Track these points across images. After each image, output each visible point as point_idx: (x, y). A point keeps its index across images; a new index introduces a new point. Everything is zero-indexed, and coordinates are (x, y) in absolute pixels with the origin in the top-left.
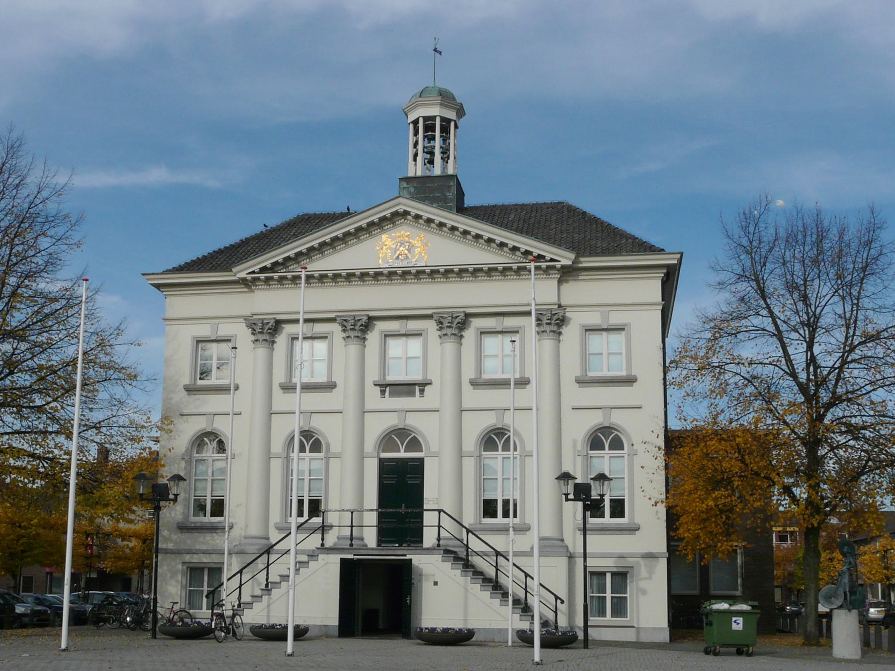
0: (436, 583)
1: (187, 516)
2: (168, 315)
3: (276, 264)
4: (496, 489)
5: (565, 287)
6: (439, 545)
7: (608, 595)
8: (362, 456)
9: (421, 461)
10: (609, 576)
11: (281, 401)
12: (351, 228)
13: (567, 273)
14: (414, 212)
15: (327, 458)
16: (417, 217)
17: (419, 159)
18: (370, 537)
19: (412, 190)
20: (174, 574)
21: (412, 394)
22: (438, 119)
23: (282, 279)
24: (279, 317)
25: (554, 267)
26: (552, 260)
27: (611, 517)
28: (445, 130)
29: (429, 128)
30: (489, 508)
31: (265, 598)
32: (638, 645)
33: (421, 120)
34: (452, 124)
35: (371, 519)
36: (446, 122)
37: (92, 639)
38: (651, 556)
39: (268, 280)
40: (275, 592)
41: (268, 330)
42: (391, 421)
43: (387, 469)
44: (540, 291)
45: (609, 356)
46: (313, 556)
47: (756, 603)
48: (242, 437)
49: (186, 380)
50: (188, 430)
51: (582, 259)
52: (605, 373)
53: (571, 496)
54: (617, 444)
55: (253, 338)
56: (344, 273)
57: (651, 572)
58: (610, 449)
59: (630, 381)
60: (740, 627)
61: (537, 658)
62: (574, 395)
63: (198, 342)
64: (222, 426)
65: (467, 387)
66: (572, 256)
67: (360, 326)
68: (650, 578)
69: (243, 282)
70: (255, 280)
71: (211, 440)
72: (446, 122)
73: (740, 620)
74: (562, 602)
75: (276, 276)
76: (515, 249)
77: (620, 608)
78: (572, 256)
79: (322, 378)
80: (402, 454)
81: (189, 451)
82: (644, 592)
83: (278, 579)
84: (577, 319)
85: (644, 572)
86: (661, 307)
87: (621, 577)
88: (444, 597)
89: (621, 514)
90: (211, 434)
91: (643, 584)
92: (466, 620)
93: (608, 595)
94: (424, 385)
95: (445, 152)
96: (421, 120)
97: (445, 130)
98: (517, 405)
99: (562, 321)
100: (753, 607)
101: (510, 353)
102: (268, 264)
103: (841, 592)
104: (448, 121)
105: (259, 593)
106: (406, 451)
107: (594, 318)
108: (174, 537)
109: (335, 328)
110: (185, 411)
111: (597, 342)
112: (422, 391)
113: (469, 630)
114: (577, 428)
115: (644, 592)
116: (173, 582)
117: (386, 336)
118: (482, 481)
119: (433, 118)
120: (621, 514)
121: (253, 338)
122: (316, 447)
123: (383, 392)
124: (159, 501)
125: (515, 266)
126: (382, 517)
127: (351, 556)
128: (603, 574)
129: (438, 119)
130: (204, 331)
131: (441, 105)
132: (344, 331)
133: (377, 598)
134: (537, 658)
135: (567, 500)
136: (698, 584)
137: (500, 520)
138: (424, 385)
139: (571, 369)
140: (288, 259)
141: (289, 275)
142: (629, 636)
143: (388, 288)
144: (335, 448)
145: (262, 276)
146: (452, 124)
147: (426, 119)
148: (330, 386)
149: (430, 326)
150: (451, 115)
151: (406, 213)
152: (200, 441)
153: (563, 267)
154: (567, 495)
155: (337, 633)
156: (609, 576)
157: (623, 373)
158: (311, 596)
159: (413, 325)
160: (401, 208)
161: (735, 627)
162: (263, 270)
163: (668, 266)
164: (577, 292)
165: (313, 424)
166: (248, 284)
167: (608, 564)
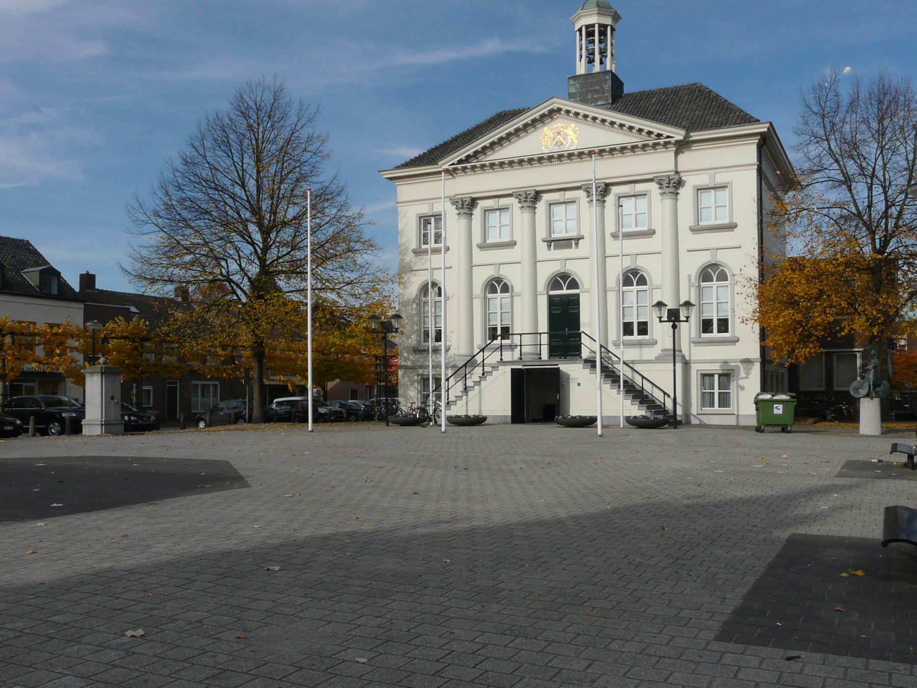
0: (579, 384)
1: (419, 342)
2: (399, 200)
3: (468, 157)
4: (632, 315)
5: (681, 157)
6: (521, 359)
7: (716, 391)
8: (535, 295)
9: (577, 296)
10: (716, 377)
11: (479, 256)
12: (528, 120)
13: (682, 146)
14: (565, 108)
15: (512, 297)
16: (568, 112)
17: (583, 59)
18: (545, 355)
19: (578, 85)
20: (412, 383)
21: (570, 247)
22: (597, 26)
23: (473, 168)
24: (608, 181)
25: (669, 143)
26: (668, 137)
27: (719, 332)
28: (603, 33)
29: (590, 34)
30: (628, 329)
31: (464, 397)
32: (738, 427)
33: (584, 28)
34: (609, 28)
35: (545, 339)
36: (602, 28)
37: (321, 426)
38: (747, 361)
39: (464, 169)
40: (471, 393)
41: (468, 205)
42: (556, 268)
43: (553, 302)
44: (661, 162)
45: (715, 209)
46: (495, 367)
47: (794, 394)
48: (453, 284)
49: (414, 246)
50: (415, 282)
51: (691, 134)
52: (713, 222)
53: (665, 318)
54: (723, 277)
55: (457, 212)
56: (607, 149)
57: (748, 374)
58: (717, 280)
59: (731, 227)
60: (780, 412)
61: (599, 433)
62: (688, 240)
63: (550, 204)
64: (439, 277)
65: (475, 250)
66: (683, 132)
67: (532, 198)
68: (747, 378)
69: (447, 171)
70: (455, 170)
71: (431, 288)
72: (602, 28)
73: (781, 407)
74: (669, 396)
75: (469, 165)
76: (640, 131)
77: (725, 401)
78: (683, 132)
79: (506, 239)
80: (565, 291)
81: (418, 296)
82: (742, 388)
83: (472, 384)
84: (691, 181)
85: (742, 374)
86: (756, 167)
87: (726, 376)
88: (586, 393)
89: (726, 331)
90: (635, 272)
91: (741, 382)
92: (480, 411)
93: (716, 391)
94: (578, 239)
95: (603, 53)
96: (584, 28)
97: (603, 33)
98: (624, 253)
99: (680, 183)
100: (792, 397)
101: (508, 223)
102: (463, 157)
103: (866, 385)
104: (605, 26)
105: (460, 394)
106: (567, 289)
107: (703, 180)
108: (411, 357)
109: (513, 201)
110: (415, 268)
111: (708, 198)
112: (577, 244)
113: (591, 417)
114: (691, 266)
115: (742, 388)
116: (412, 389)
117: (619, 198)
118: (486, 316)
119: (593, 26)
120: (726, 331)
121: (457, 212)
122: (505, 289)
123: (549, 246)
124: (386, 333)
125: (640, 144)
126: (551, 337)
127: (520, 367)
128: (712, 375)
129: (597, 26)
130: (424, 209)
131: (598, 14)
132: (660, 188)
133: (538, 396)
134: (310, 429)
135: (661, 321)
136: (824, 378)
137: (715, 334)
138: (578, 239)
139: (686, 219)
140: (476, 153)
141: (478, 164)
142: (731, 421)
143: (621, 159)
144: (450, 293)
145: (459, 166)
146: (609, 28)
147: (587, 27)
148: (512, 244)
149: (653, 187)
150: (608, 21)
151: (559, 110)
152: (424, 290)
153: (677, 142)
154: (660, 318)
155: (510, 420)
156: (716, 377)
157: (726, 221)
158: (494, 397)
159: (569, 195)
160: (555, 106)
161: (776, 411)
162: (460, 162)
163: (761, 134)
164: (688, 160)
165: (718, 258)
166: (452, 172)
167: (715, 368)
